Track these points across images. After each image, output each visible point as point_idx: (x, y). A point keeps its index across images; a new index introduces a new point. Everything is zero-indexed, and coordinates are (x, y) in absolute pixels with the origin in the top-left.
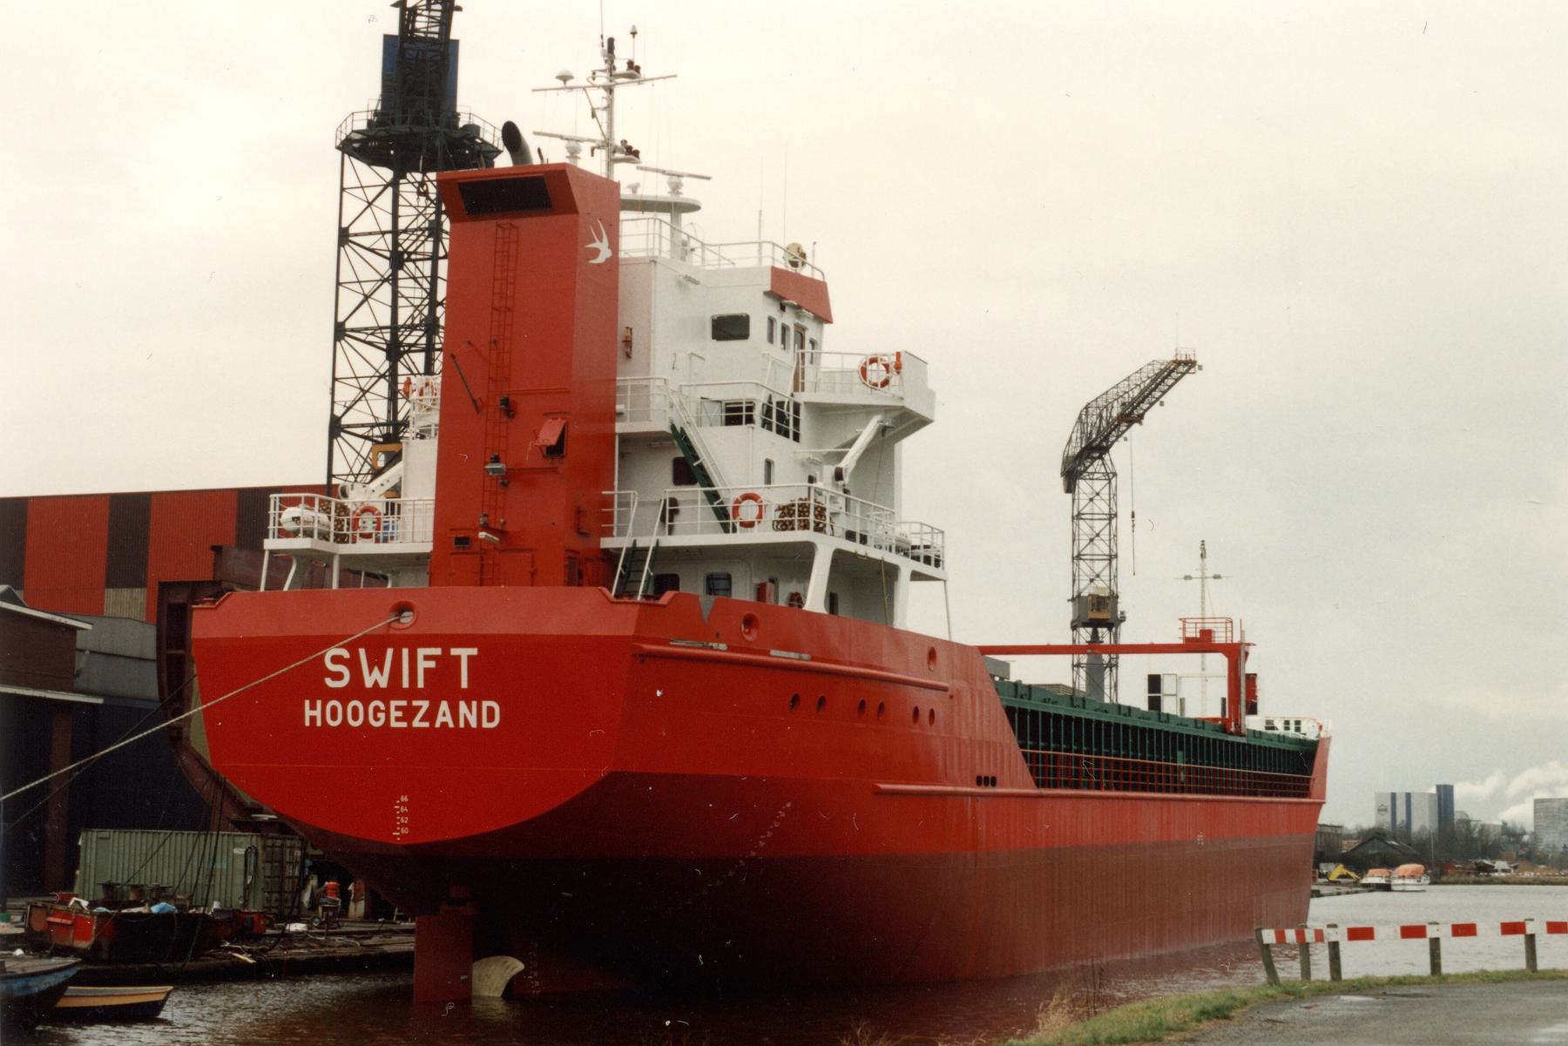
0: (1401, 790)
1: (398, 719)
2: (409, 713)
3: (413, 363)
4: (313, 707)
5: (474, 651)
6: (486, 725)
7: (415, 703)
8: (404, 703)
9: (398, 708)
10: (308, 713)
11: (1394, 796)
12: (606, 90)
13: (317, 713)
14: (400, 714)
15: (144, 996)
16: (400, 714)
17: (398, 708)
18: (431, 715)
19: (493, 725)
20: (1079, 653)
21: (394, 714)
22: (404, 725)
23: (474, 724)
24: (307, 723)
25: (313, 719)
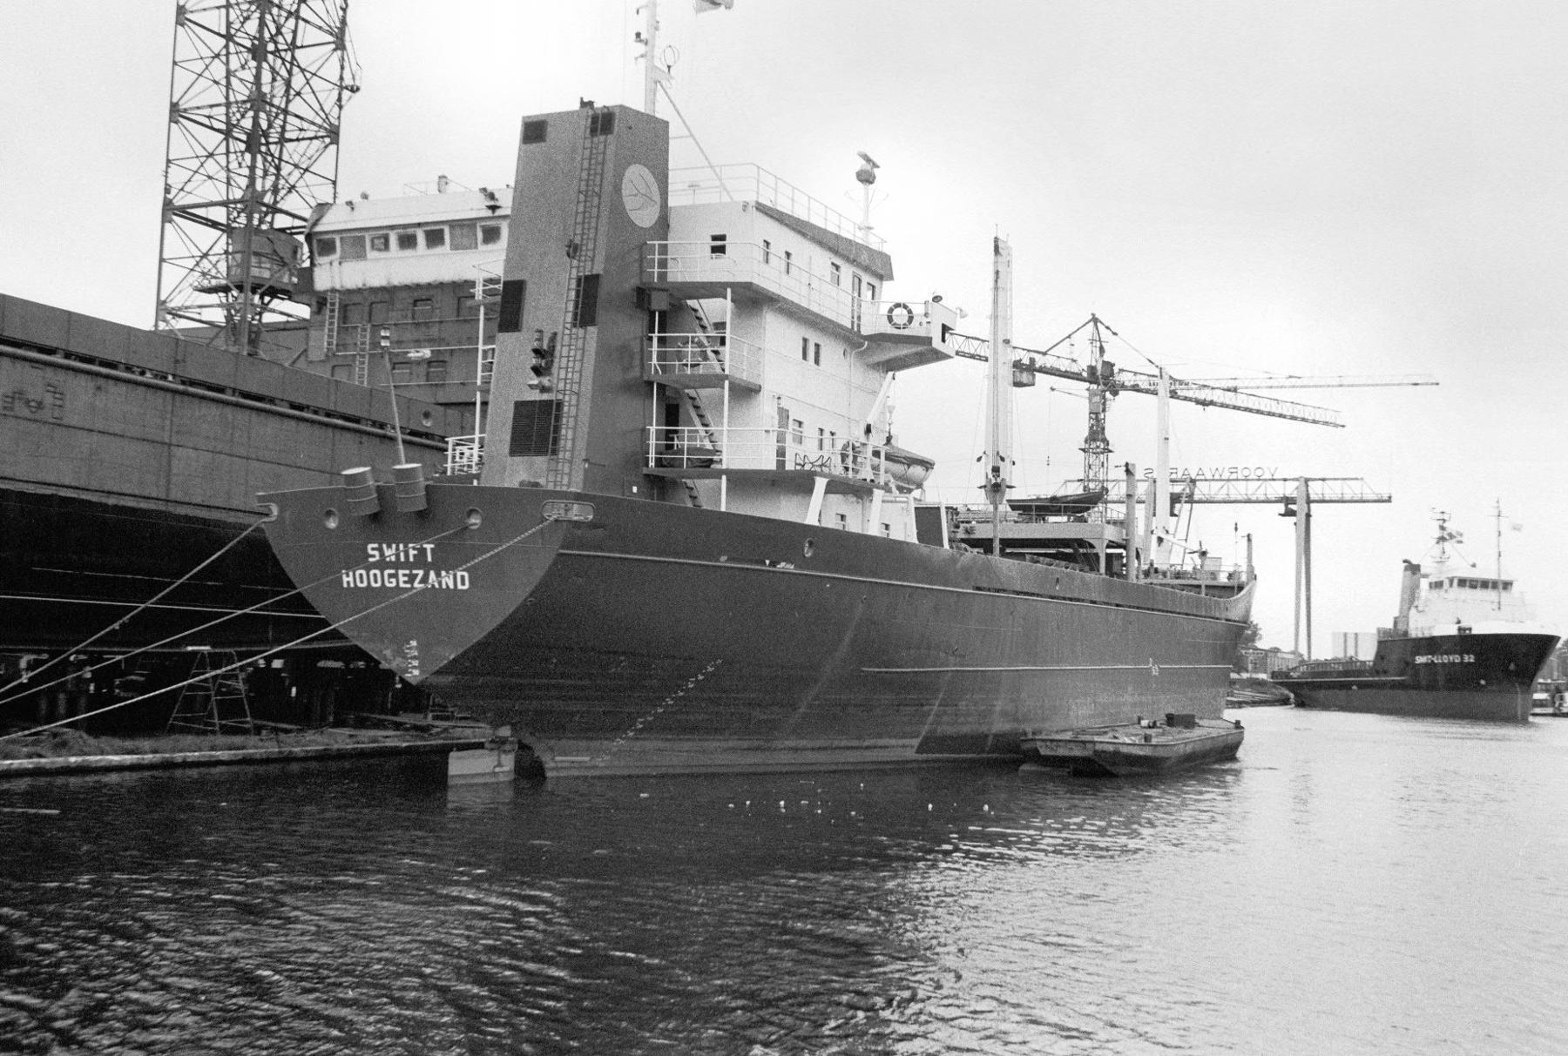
0: (1351, 631)
1: (405, 582)
2: (412, 578)
3: (1297, 635)
4: (348, 576)
5: (432, 546)
6: (460, 587)
7: (415, 572)
8: (407, 572)
9: (404, 575)
10: (345, 579)
11: (1345, 635)
12: (1243, 617)
13: (351, 579)
14: (406, 579)
15: (1353, 644)
16: (406, 579)
17: (404, 575)
18: (425, 580)
19: (466, 587)
20: (554, 492)
21: (402, 579)
22: (409, 586)
23: (452, 587)
24: (345, 585)
25: (348, 583)
